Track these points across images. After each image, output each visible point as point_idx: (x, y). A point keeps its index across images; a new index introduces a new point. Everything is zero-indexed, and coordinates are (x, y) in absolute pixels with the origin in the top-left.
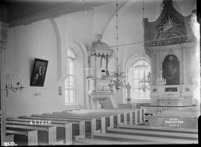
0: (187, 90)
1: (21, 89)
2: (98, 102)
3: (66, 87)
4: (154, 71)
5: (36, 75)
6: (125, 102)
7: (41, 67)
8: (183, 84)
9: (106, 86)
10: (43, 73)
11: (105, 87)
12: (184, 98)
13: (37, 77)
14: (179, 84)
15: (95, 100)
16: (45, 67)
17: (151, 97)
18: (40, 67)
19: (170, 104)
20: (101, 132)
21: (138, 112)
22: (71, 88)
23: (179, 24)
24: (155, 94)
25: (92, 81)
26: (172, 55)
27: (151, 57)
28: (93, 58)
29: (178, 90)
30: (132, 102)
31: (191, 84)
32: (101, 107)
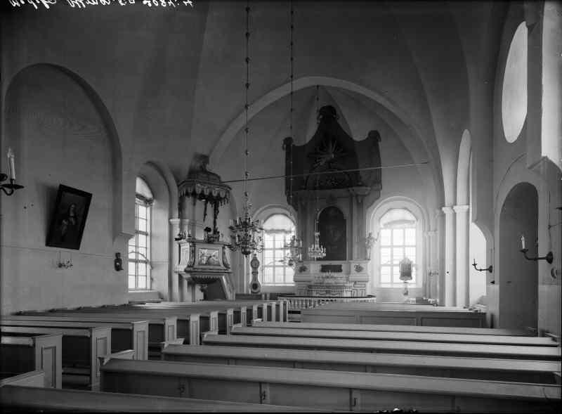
0: (359, 269)
1: (8, 191)
2: (198, 288)
3: (132, 256)
4: (302, 235)
5: (60, 223)
6: (247, 290)
7: (73, 206)
8: (352, 259)
9: (214, 256)
10: (80, 219)
11: (213, 258)
12: (353, 283)
13: (65, 228)
14: (344, 259)
15: (192, 283)
16: (83, 209)
17: (296, 281)
18: (70, 206)
19: (331, 292)
20: (262, 321)
21: (278, 306)
22: (141, 258)
23: (344, 154)
24: (304, 276)
25: (186, 247)
26: (333, 207)
27: (297, 210)
28: (188, 201)
29: (518, 180)
30: (262, 290)
31: (366, 259)
32: (202, 298)
